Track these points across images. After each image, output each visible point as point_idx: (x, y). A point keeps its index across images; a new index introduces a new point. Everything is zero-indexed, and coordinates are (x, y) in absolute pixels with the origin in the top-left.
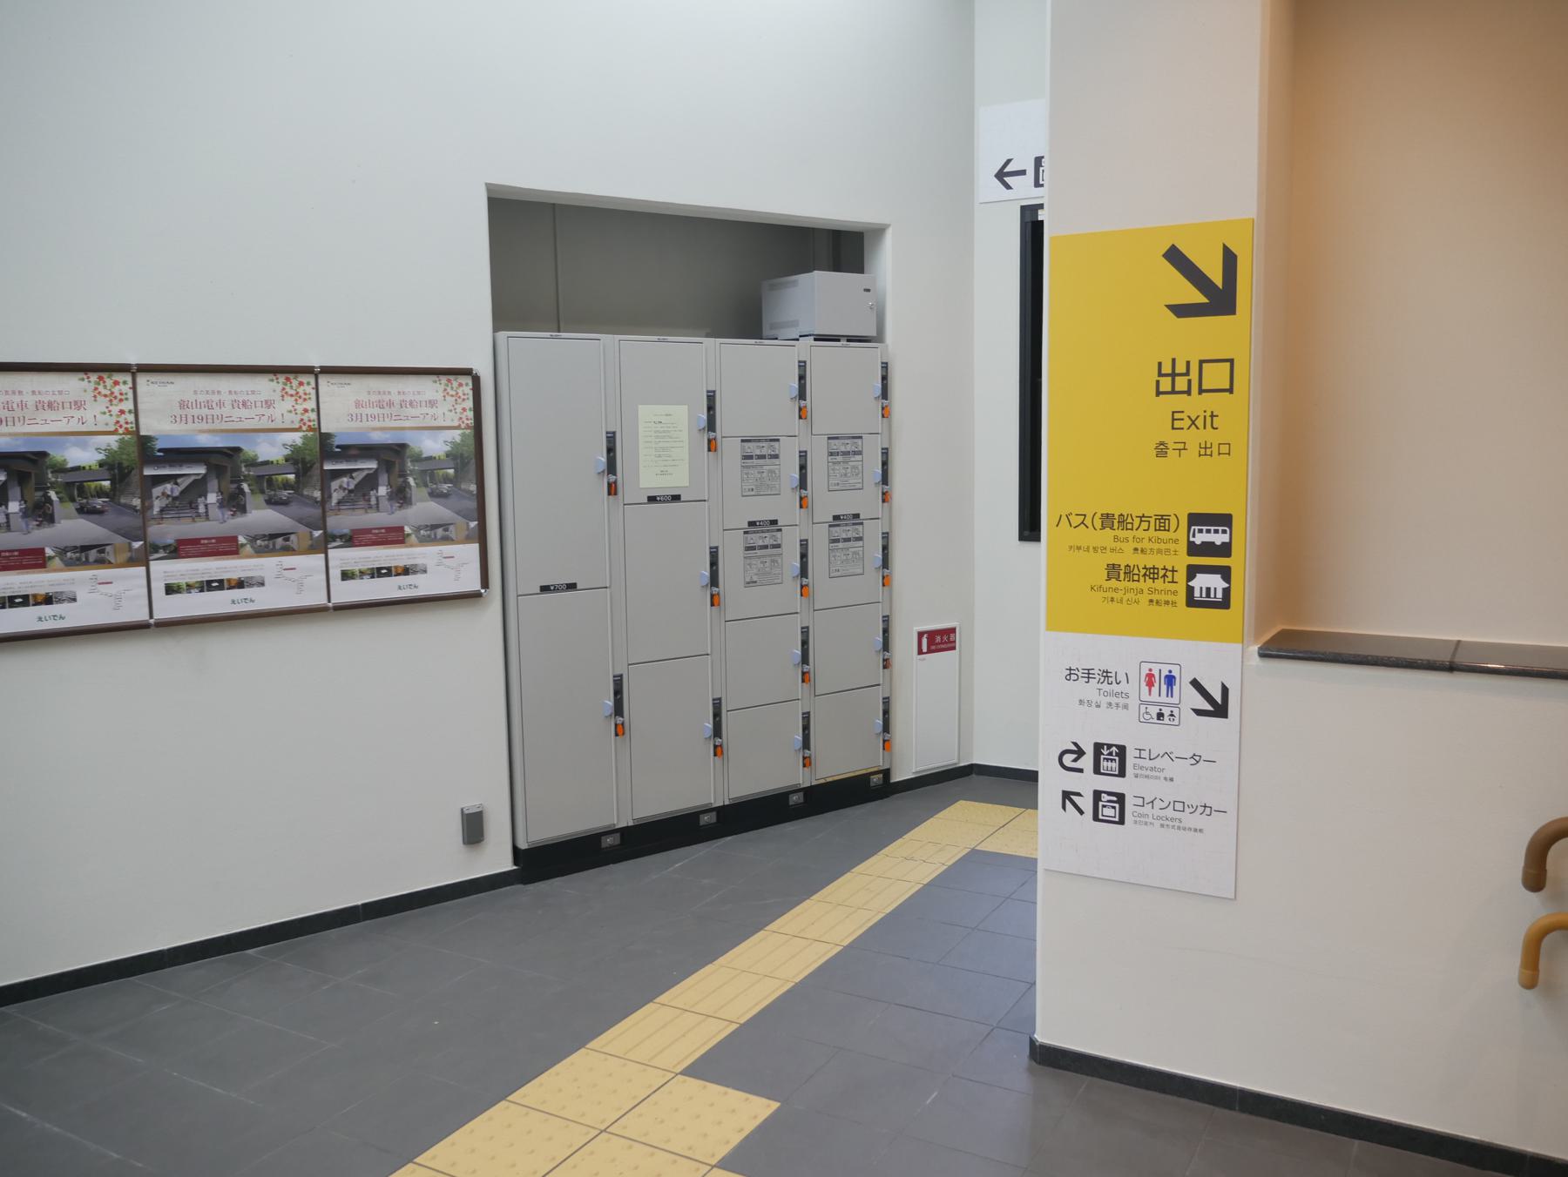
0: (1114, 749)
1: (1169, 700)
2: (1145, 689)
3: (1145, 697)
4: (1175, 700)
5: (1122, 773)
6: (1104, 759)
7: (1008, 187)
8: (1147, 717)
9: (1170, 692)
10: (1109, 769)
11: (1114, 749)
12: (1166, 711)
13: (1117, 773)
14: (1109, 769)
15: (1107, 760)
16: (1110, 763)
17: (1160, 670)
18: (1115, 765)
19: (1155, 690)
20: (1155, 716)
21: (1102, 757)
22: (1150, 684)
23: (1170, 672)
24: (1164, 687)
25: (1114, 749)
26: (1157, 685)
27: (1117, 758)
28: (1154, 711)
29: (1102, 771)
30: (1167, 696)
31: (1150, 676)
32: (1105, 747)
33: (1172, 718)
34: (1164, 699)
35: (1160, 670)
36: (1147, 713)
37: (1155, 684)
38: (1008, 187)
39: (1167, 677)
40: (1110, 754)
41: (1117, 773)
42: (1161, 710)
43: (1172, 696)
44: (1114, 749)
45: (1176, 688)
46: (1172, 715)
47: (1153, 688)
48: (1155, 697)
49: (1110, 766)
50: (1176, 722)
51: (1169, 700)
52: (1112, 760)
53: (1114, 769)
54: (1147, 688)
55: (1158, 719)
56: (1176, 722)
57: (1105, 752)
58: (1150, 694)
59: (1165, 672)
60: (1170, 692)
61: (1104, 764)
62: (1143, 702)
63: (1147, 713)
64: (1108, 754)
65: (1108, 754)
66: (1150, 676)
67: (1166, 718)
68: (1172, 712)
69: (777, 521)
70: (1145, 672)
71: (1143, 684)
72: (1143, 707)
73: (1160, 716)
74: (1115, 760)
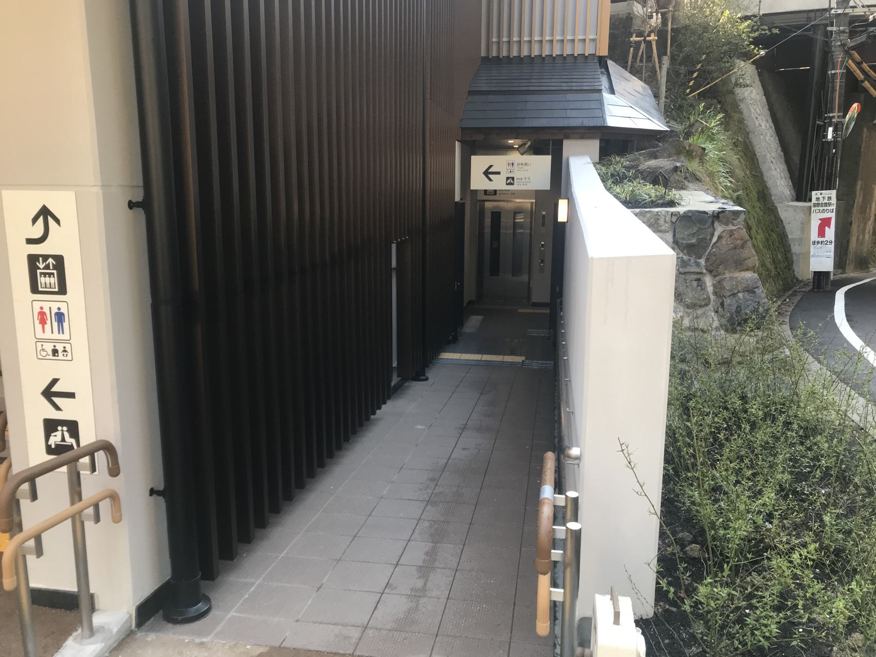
0: (50, 260)
1: (61, 337)
2: (39, 327)
3: (40, 335)
4: (66, 336)
5: (63, 290)
6: (41, 273)
7: (490, 180)
8: (44, 354)
9: (61, 329)
10: (48, 285)
11: (51, 261)
12: (60, 347)
13: (57, 290)
14: (48, 285)
15: (45, 274)
16: (47, 279)
17: (50, 308)
18: (54, 280)
19: (48, 327)
20: (50, 353)
21: (39, 271)
22: (43, 322)
23: (59, 309)
24: (55, 324)
25: (50, 260)
26: (49, 322)
27: (55, 272)
28: (49, 347)
29: (40, 289)
30: (59, 333)
31: (42, 314)
32: (41, 259)
33: (65, 353)
34: (56, 336)
35: (50, 308)
36: (43, 350)
37: (47, 322)
38: (490, 180)
39: (56, 314)
40: (47, 267)
41: (57, 290)
42: (55, 346)
43: (63, 333)
44: (51, 261)
45: (66, 325)
46: (65, 351)
47: (45, 325)
48: (48, 335)
49: (48, 282)
50: (69, 358)
51: (61, 337)
52: (50, 275)
53: (53, 286)
54: (41, 325)
55: (54, 355)
56: (69, 358)
57: (41, 266)
58: (44, 332)
59: (54, 310)
60: (61, 329)
61: (42, 280)
62: (39, 340)
63: (43, 350)
64: (45, 268)
65: (45, 268)
66: (42, 314)
67: (60, 354)
68: (64, 347)
69: (544, 226)
70: (37, 310)
71: (37, 322)
72: (39, 344)
73: (55, 352)
74: (53, 274)
